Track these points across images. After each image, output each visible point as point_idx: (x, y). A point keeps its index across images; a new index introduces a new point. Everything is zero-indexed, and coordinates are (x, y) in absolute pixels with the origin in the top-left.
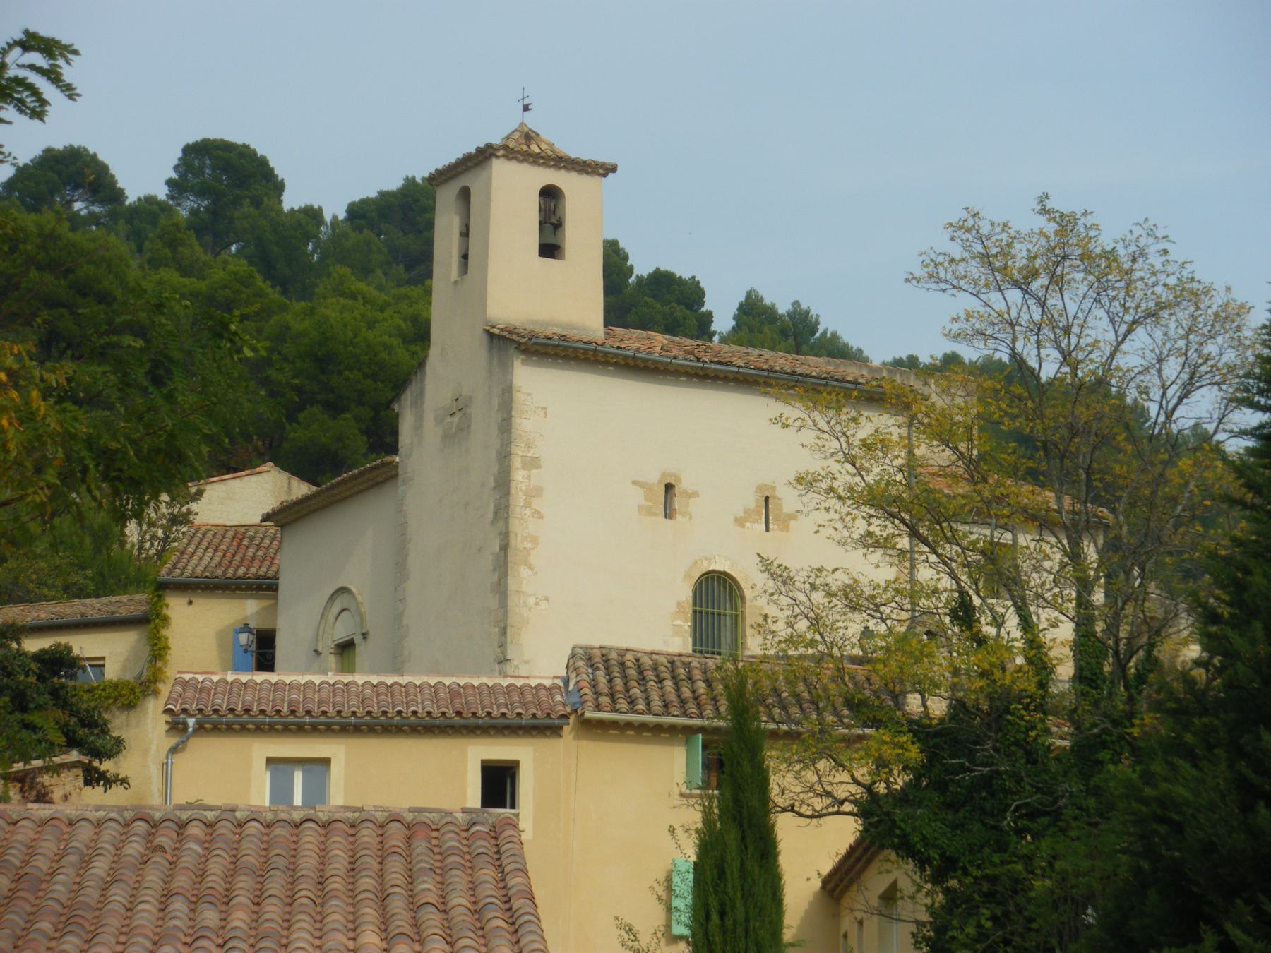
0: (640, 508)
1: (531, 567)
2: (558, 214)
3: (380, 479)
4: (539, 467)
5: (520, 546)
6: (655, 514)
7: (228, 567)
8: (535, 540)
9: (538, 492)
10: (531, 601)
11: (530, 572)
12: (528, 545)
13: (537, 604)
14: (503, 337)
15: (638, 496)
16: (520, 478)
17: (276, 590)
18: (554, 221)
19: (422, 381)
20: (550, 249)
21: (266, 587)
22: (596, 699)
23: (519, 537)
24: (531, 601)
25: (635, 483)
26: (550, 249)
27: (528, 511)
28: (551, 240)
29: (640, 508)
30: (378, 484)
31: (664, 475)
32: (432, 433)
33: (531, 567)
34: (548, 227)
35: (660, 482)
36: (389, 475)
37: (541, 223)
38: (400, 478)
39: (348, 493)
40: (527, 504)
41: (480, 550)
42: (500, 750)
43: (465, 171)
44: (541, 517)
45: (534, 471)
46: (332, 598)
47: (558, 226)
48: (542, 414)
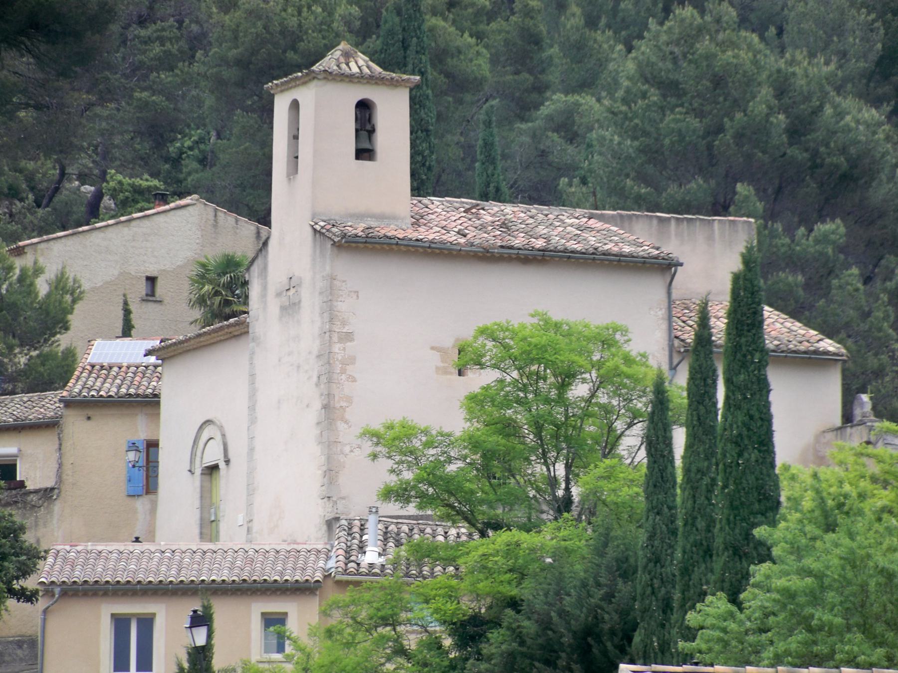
0: (437, 368)
1: (346, 422)
2: (374, 121)
3: (236, 333)
4: (352, 340)
5: (337, 405)
6: (451, 373)
7: (119, 387)
8: (349, 399)
9: (352, 360)
10: (347, 449)
11: (346, 426)
12: (344, 404)
13: (352, 451)
14: (323, 234)
15: (435, 359)
16: (337, 350)
17: (158, 403)
18: (368, 127)
19: (266, 257)
20: (364, 153)
21: (150, 403)
22: (346, 564)
23: (337, 398)
24: (347, 449)
25: (433, 348)
26: (364, 153)
27: (344, 377)
28: (366, 145)
29: (437, 368)
30: (235, 336)
31: (457, 340)
32: (274, 306)
33: (346, 422)
34: (364, 134)
35: (454, 346)
36: (241, 332)
37: (357, 131)
38: (251, 335)
39: (212, 341)
40: (343, 371)
41: (308, 406)
42: (274, 606)
43: (295, 86)
44: (354, 380)
45: (349, 344)
46: (201, 428)
47: (371, 132)
48: (355, 297)
